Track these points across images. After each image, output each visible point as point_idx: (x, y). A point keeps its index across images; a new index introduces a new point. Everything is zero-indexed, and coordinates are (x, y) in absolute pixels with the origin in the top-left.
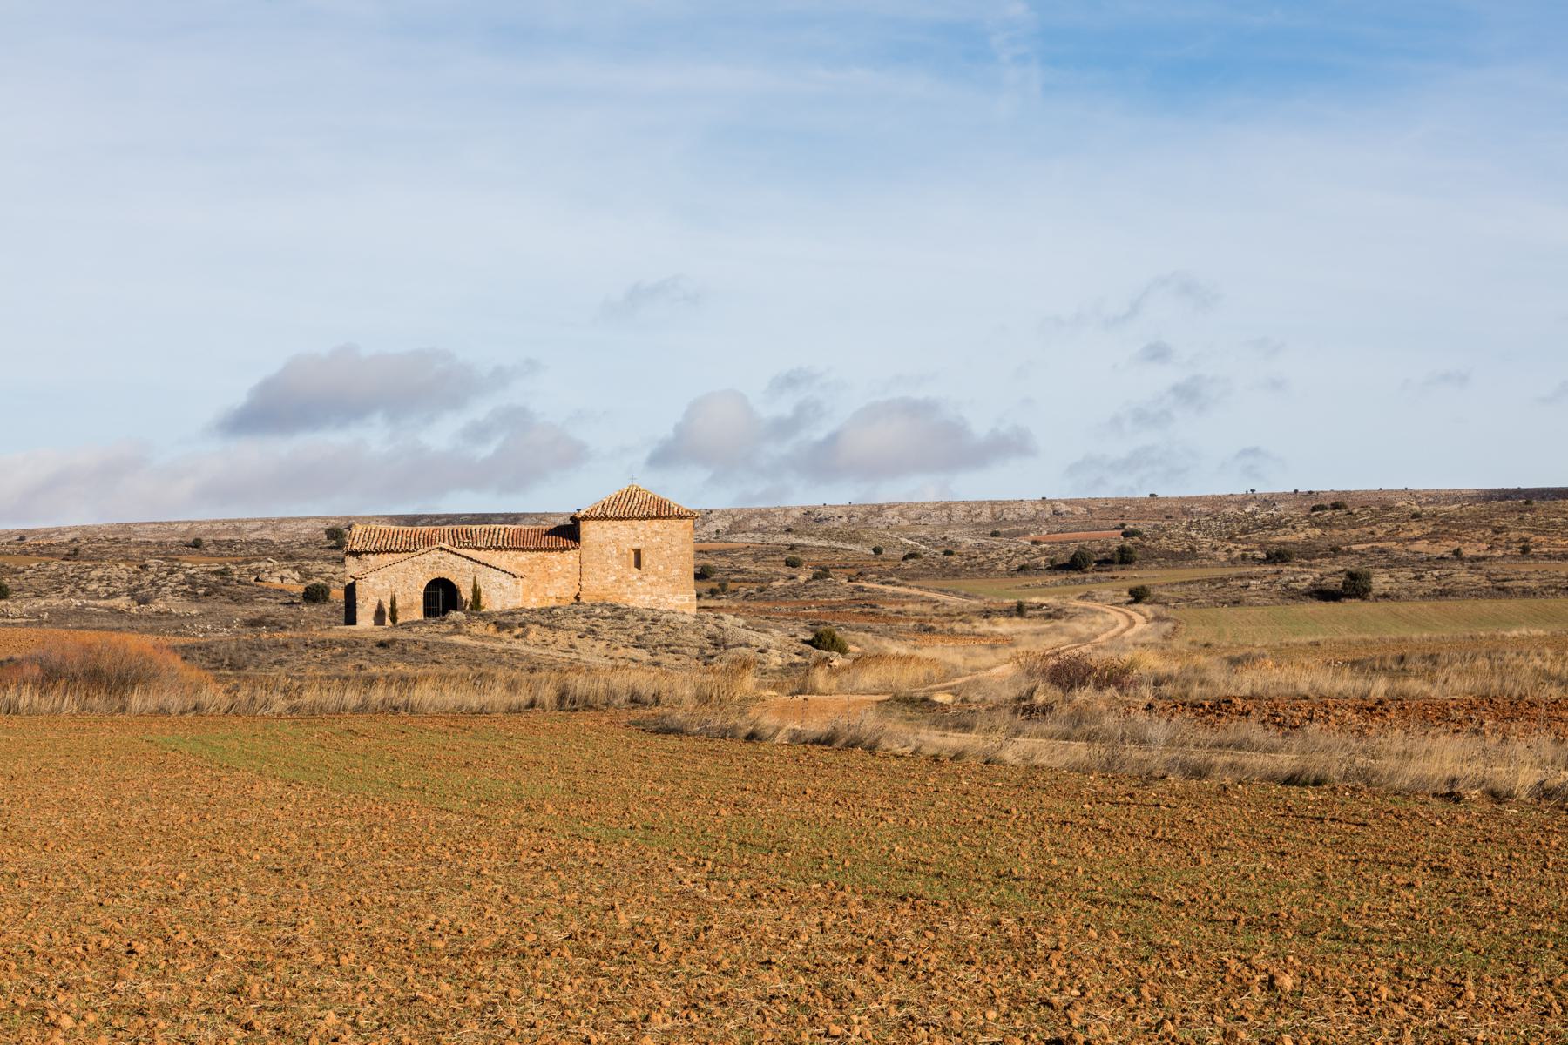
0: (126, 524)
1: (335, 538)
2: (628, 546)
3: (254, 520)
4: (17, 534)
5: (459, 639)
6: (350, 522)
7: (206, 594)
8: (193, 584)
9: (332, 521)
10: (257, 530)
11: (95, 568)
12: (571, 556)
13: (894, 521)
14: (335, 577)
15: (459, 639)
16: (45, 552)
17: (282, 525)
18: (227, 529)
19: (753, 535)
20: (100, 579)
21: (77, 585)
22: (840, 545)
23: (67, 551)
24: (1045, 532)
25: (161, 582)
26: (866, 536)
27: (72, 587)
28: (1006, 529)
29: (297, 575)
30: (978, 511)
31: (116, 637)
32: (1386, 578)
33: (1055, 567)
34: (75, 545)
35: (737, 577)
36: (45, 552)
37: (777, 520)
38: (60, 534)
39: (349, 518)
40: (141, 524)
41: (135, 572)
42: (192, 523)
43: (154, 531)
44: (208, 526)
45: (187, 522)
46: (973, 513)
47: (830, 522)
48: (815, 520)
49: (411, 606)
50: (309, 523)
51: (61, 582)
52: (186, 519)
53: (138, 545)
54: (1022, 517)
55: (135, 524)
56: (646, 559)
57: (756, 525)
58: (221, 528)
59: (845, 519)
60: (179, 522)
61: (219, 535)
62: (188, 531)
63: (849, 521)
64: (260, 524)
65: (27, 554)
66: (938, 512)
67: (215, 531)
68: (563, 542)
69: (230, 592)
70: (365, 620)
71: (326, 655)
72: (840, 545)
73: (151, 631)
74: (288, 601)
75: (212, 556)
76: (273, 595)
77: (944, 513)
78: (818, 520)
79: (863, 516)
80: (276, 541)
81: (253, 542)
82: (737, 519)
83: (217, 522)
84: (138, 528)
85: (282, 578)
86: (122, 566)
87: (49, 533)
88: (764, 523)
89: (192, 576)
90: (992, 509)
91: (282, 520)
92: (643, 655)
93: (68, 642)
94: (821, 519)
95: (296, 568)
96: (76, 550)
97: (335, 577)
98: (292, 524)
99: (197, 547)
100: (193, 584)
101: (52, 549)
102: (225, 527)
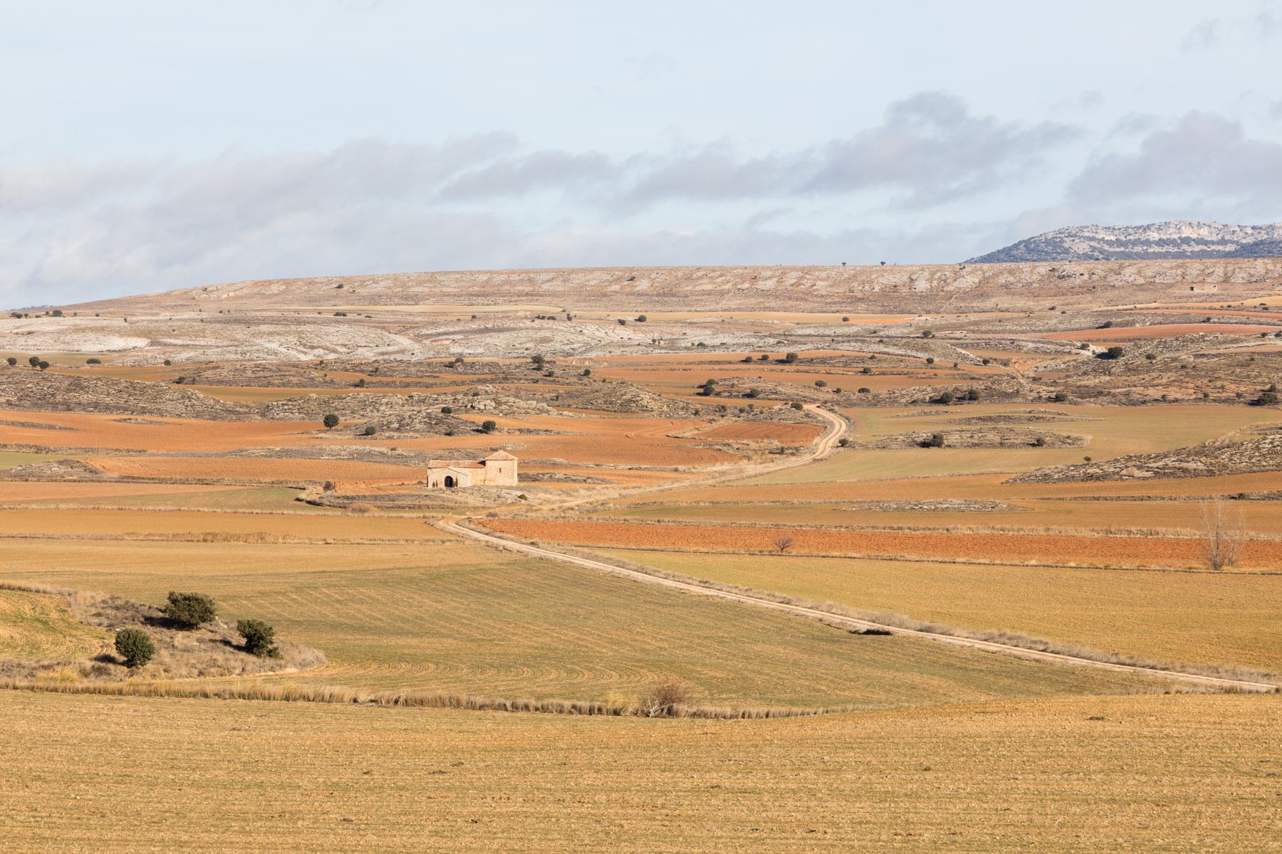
0: (433, 273)
1: (538, 362)
2: (498, 467)
3: (547, 271)
4: (336, 282)
5: (443, 495)
6: (633, 274)
7: (436, 424)
8: (430, 418)
9: (617, 273)
10: (549, 281)
11: (384, 397)
12: (483, 469)
13: (1130, 279)
14: (515, 405)
15: (443, 495)
16: (358, 369)
17: (572, 277)
18: (522, 280)
19: (854, 344)
20: (387, 404)
21: (374, 407)
22: (914, 353)
23: (371, 369)
24: (1148, 323)
25: (414, 417)
26: (933, 347)
27: (371, 408)
28: (1120, 320)
29: (493, 404)
30: (1211, 270)
31: (382, 466)
32: (958, 437)
33: (934, 401)
34: (376, 365)
35: (773, 396)
36: (358, 369)
37: (1023, 276)
38: (374, 283)
39: (632, 269)
40: (446, 273)
41: (406, 400)
42: (491, 272)
43: (457, 280)
44: (504, 277)
45: (486, 272)
46: (1206, 272)
47: (1072, 279)
48: (1059, 277)
49: (441, 483)
50: (596, 274)
51: (365, 405)
52: (486, 268)
53: (415, 365)
54: (1252, 276)
55: (440, 273)
56: (502, 470)
57: (1004, 281)
58: (517, 278)
59: (1086, 277)
60: (480, 272)
61: (514, 285)
62: (487, 281)
63: (1090, 278)
64: (551, 275)
65: (346, 370)
66: (1174, 271)
67: (511, 282)
68: (482, 466)
69: (447, 423)
70: (430, 486)
71: (413, 498)
72: (914, 353)
73: (395, 463)
74: (476, 428)
75: (461, 374)
76: (469, 425)
77: (1179, 272)
78: (1061, 278)
79: (1103, 274)
80: (501, 364)
81: (487, 364)
82: (987, 275)
83: (514, 272)
84: (442, 278)
85: (485, 405)
86: (399, 396)
87: (364, 282)
88: (1011, 279)
89: (429, 414)
90: (1225, 268)
91: (572, 271)
92: (482, 499)
93: (296, 652)
94: (1063, 277)
95: (494, 399)
96: (377, 369)
97: (515, 405)
98: (580, 276)
99: (451, 367)
100: (430, 418)
101: (362, 367)
102: (521, 277)
